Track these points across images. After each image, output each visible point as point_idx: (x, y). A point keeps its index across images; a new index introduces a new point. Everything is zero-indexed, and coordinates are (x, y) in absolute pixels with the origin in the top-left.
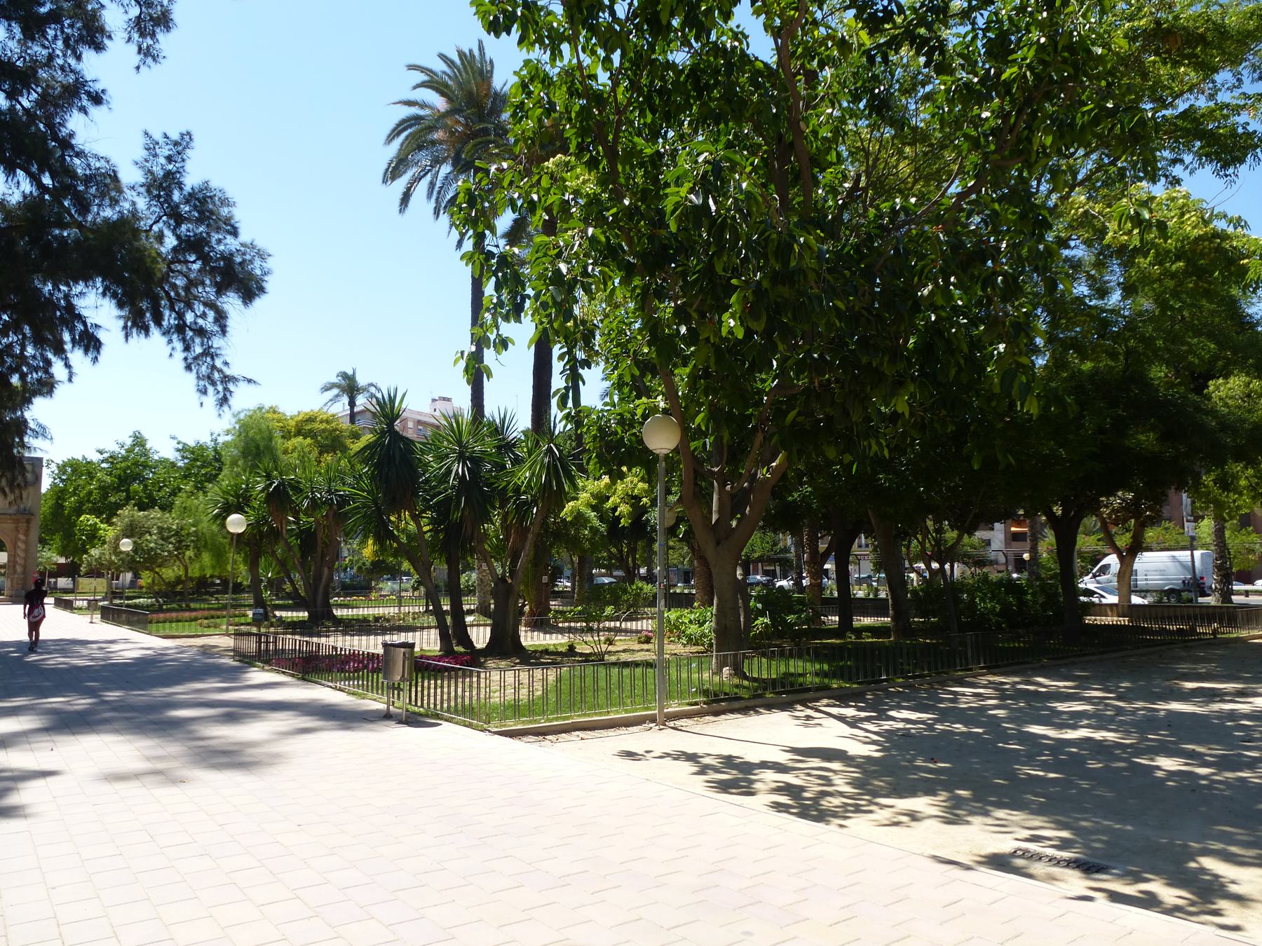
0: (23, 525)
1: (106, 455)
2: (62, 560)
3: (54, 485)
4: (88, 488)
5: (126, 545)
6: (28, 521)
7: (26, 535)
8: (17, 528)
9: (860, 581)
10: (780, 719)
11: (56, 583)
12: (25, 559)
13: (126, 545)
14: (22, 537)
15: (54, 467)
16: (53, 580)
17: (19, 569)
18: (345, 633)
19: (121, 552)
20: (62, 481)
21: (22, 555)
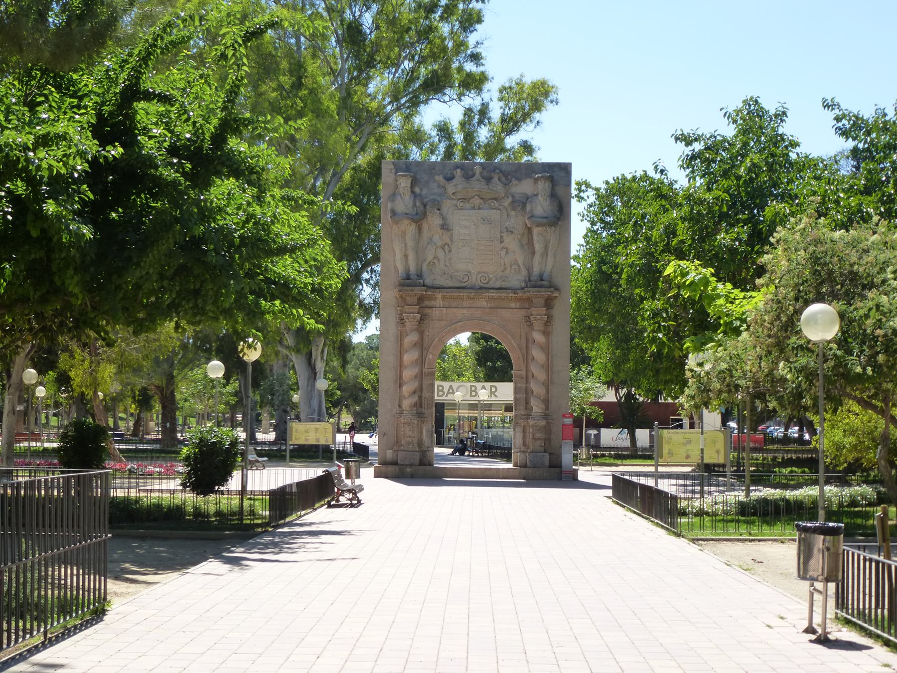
0: (539, 312)
1: (698, 147)
2: (610, 396)
3: (591, 234)
4: (664, 219)
5: (820, 323)
6: (549, 304)
7: (546, 333)
8: (528, 318)
9: (137, 483)
10: (844, 639)
11: (598, 436)
12: (547, 385)
13: (820, 323)
14: (538, 337)
15: (590, 196)
16: (593, 432)
17: (537, 407)
18: (142, 461)
19: (807, 348)
20: (607, 226)
21: (540, 375)
